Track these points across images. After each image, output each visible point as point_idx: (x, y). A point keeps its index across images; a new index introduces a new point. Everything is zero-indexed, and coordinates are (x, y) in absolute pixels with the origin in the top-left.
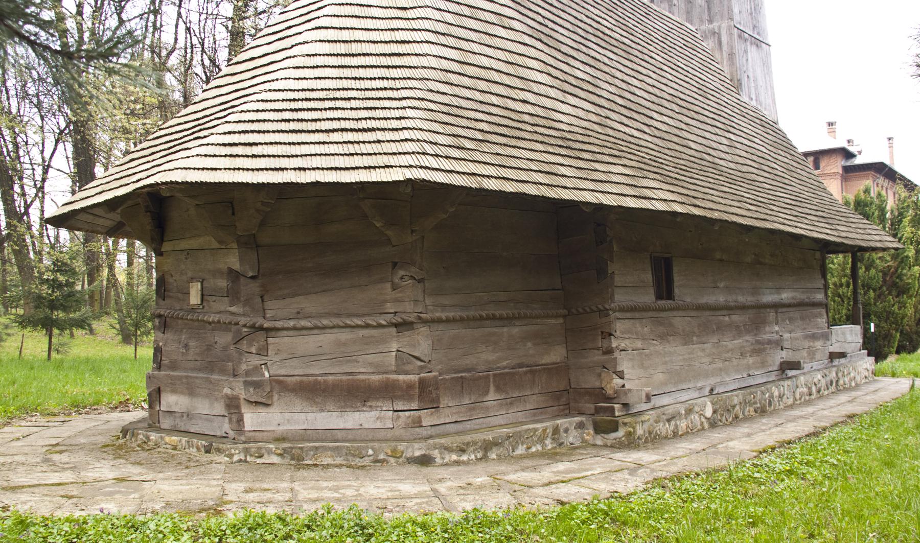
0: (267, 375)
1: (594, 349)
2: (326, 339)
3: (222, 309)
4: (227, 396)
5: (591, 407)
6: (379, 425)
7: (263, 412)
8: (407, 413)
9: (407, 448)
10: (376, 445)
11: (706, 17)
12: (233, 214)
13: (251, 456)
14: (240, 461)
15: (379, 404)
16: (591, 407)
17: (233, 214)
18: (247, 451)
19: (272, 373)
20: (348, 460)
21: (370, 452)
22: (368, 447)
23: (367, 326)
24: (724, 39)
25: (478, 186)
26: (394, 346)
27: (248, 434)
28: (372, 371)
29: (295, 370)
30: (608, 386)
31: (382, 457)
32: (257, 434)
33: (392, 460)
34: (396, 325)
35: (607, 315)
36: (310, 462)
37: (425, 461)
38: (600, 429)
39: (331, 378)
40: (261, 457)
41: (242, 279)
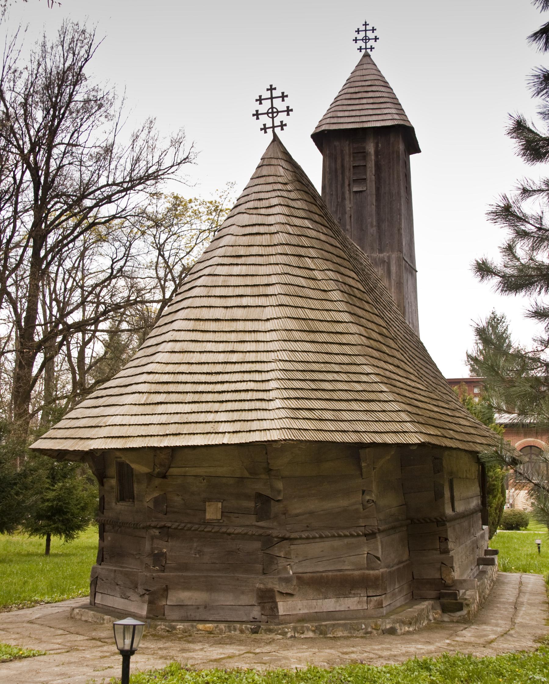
0: (291, 573)
1: (433, 549)
2: (326, 545)
3: (248, 523)
4: (259, 590)
5: (434, 593)
6: (359, 607)
7: (290, 602)
8: (375, 598)
9: (382, 623)
10: (366, 622)
11: (376, 246)
12: (266, 453)
13: (298, 632)
14: (292, 637)
15: (359, 592)
16: (434, 593)
17: (266, 453)
18: (295, 629)
19: (295, 571)
20: (351, 633)
21: (363, 626)
22: (361, 623)
23: (352, 536)
24: (394, 269)
25: (86, 356)
26: (366, 550)
27: (281, 618)
28: (353, 568)
29: (308, 568)
30: (447, 578)
31: (369, 630)
32: (287, 617)
33: (375, 632)
34: (365, 535)
35: (445, 525)
36: (331, 636)
37: (392, 632)
38: (445, 609)
39: (330, 573)
40: (303, 633)
41: (272, 502)
